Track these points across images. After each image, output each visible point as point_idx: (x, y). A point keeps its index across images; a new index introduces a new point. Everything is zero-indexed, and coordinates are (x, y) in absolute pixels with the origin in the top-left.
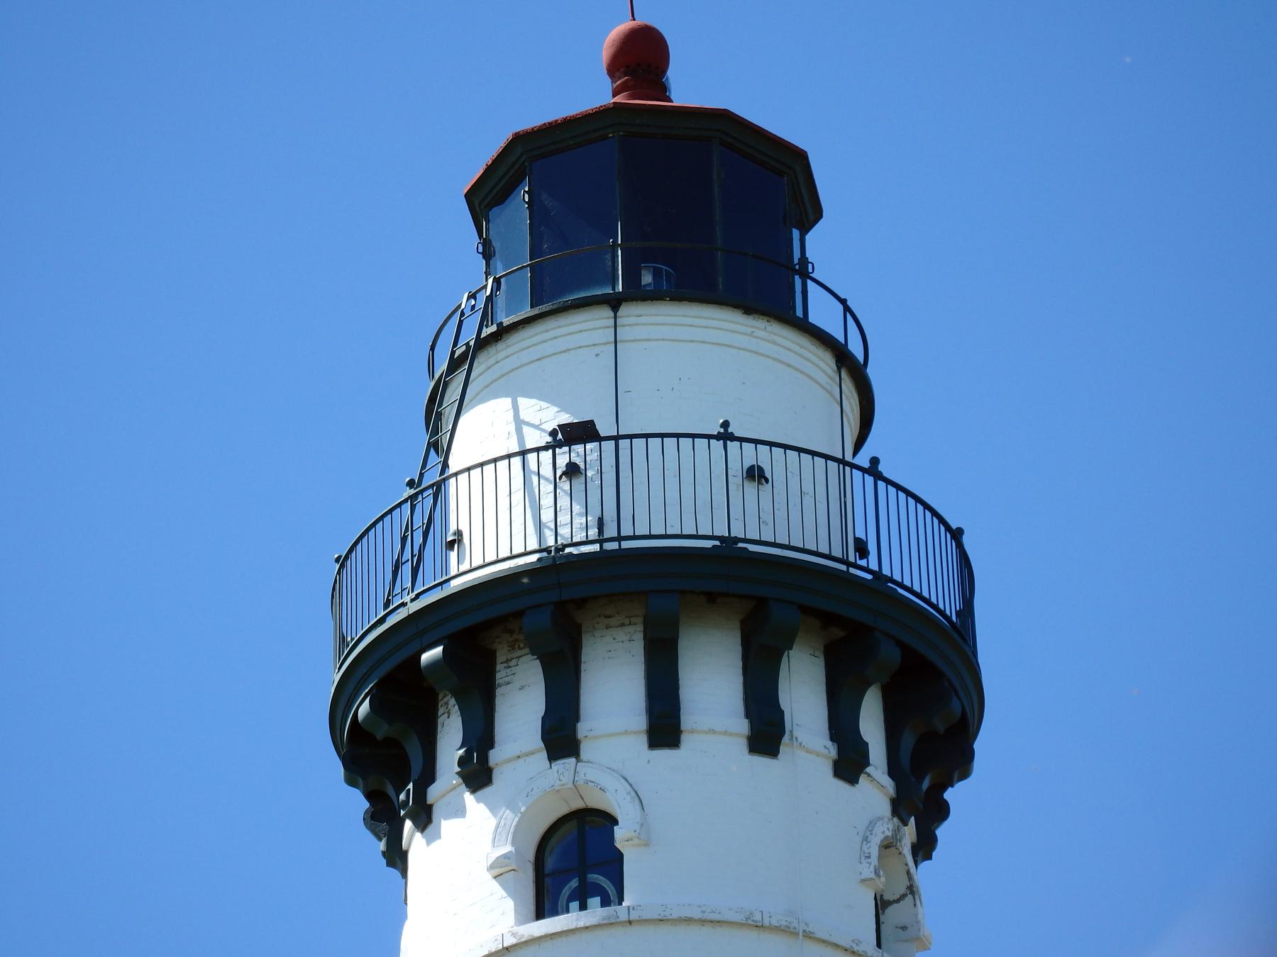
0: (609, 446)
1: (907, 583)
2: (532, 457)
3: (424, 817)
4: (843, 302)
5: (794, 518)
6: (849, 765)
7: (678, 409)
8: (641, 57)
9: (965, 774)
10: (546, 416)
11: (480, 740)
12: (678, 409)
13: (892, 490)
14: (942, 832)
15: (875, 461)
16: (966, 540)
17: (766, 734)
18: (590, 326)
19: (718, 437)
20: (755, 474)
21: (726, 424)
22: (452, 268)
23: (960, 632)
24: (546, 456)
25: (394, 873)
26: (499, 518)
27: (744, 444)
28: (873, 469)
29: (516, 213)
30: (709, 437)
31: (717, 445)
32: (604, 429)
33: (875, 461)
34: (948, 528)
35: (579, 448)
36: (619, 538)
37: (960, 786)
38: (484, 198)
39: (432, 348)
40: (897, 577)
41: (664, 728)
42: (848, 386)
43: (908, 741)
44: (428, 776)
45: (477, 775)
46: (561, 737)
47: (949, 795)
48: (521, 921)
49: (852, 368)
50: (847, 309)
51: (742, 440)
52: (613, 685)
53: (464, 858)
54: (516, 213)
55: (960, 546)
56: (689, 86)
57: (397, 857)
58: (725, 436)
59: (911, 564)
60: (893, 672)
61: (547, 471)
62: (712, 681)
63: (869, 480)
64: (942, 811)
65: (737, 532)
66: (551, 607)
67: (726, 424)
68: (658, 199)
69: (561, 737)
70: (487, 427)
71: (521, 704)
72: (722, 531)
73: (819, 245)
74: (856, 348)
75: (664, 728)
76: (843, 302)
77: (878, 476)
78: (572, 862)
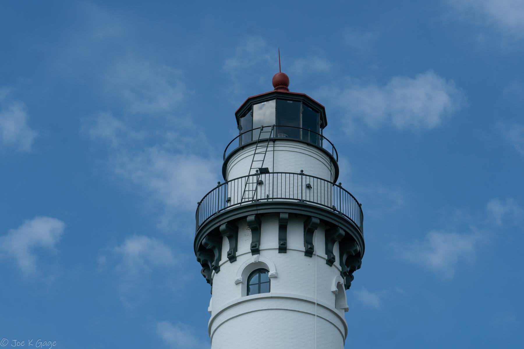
0: (271, 175)
1: (347, 215)
2: (251, 177)
3: (217, 269)
4: (333, 145)
5: (320, 196)
6: (330, 262)
7: (288, 170)
9: (359, 267)
11: (234, 249)
12: (288, 170)
13: (344, 192)
14: (352, 283)
15: (340, 184)
16: (362, 207)
17: (309, 252)
19: (300, 174)
20: (309, 187)
21: (302, 171)
23: (358, 231)
24: (255, 177)
25: (209, 285)
27: (257, 285)
28: (340, 186)
30: (298, 174)
31: (300, 176)
32: (271, 170)
33: (340, 184)
34: (358, 203)
35: (263, 175)
36: (273, 199)
37: (357, 271)
39: (225, 151)
40: (345, 213)
41: (283, 249)
42: (333, 167)
43: (345, 257)
44: (220, 259)
46: (255, 250)
47: (353, 274)
48: (242, 296)
49: (334, 163)
50: (334, 147)
51: (306, 175)
53: (229, 276)
55: (360, 208)
57: (210, 281)
58: (302, 174)
59: (348, 209)
60: (342, 239)
61: (255, 181)
62: (296, 239)
63: (339, 188)
64: (352, 278)
65: (304, 199)
67: (302, 171)
69: (255, 250)
71: (245, 243)
72: (300, 198)
73: (326, 132)
74: (335, 157)
76: (333, 145)
77: (341, 188)
78: (257, 278)
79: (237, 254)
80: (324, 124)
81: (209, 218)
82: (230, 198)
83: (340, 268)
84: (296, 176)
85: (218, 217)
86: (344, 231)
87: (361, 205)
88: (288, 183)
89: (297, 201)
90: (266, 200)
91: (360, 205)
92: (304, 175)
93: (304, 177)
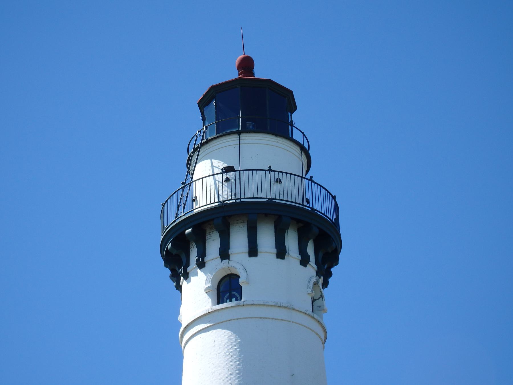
3: (186, 276)
4: (303, 133)
5: (289, 193)
6: (304, 261)
8: (246, 65)
10: (220, 165)
15: (311, 177)
16: (337, 199)
17: (281, 253)
18: (232, 140)
19: (268, 170)
20: (278, 181)
21: (270, 167)
22: (194, 123)
23: (335, 224)
24: (220, 176)
25: (178, 292)
26: (207, 191)
28: (311, 179)
29: (212, 107)
30: (265, 170)
31: (268, 173)
33: (311, 177)
34: (332, 195)
37: (335, 267)
38: (203, 104)
39: (189, 146)
41: (253, 251)
42: (304, 156)
43: (321, 255)
44: (188, 265)
45: (201, 264)
46: (224, 254)
47: (331, 270)
48: (213, 305)
49: (305, 151)
50: (304, 135)
51: (274, 171)
52: (239, 239)
54: (212, 107)
55: (335, 201)
56: (260, 73)
57: (179, 287)
58: (270, 170)
59: (321, 206)
60: (317, 237)
61: (220, 180)
62: (266, 238)
63: (310, 182)
64: (330, 274)
65: (273, 197)
66: (221, 218)
67: (270, 167)
68: (251, 104)
69: (224, 254)
70: (203, 168)
71: (213, 245)
73: (296, 117)
74: (306, 145)
75: (253, 251)
76: (303, 133)
78: (227, 289)
79: (206, 259)
80: (293, 108)
81: (174, 222)
82: (196, 197)
83: (315, 266)
84: (263, 172)
85: (185, 223)
86: (319, 228)
87: (335, 197)
88: (255, 186)
89: (265, 200)
90: (234, 201)
91: (334, 197)
92: (272, 171)
93: (272, 173)
